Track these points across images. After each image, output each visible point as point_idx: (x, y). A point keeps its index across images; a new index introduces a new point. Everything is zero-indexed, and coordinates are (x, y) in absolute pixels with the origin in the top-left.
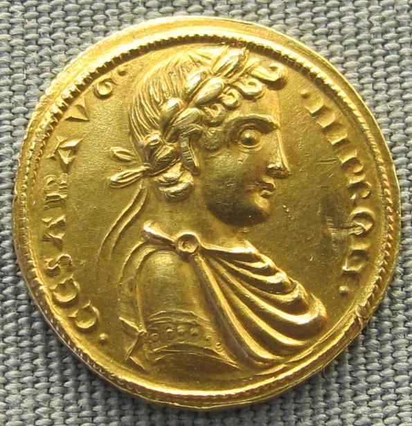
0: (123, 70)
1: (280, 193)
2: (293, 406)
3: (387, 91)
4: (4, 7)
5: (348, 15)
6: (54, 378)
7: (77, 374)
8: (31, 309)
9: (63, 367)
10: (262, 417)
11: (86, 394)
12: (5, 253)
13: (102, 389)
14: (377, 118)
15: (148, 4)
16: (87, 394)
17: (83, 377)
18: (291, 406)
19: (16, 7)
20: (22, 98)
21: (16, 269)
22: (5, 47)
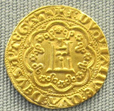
0: (26, 32)
1: (9, 69)
2: (82, 106)
3: (105, 24)
4: (1, 107)
5: (93, 8)
6: (12, 92)
7: (22, 100)
8: (7, 77)
9: (18, 97)
10: (74, 109)
11: (6, 78)
12: (1, 65)
13: (32, 106)
14: (103, 31)
15: (44, 1)
16: (20, 97)
17: (23, 101)
18: (81, 106)
19: (7, 5)
20: (8, 33)
21: (4, 67)
22: (2, 103)
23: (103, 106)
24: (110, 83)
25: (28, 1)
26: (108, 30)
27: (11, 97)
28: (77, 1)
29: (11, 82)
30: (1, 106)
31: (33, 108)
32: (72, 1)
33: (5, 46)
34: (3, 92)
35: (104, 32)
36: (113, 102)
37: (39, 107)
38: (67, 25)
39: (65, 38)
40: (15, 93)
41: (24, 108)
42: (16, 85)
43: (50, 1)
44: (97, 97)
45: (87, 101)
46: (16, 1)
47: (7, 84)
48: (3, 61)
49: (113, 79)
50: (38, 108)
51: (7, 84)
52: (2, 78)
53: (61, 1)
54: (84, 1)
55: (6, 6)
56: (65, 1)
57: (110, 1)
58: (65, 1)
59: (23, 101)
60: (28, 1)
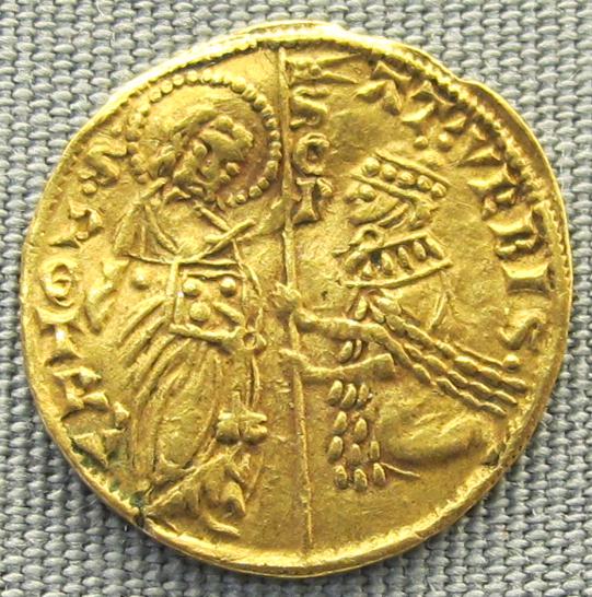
17: (152, 558)
22: (6, 83)
24: (553, 484)
26: (512, 27)
29: (30, 399)
30: (8, 69)
31: (203, 583)
32: (171, 5)
35: (530, 113)
38: (146, 353)
39: (172, 333)
40: (86, 509)
42: (51, 411)
44: (480, 526)
47: (28, 447)
49: (590, 466)
50: (227, 583)
51: (28, 447)
56: (561, 5)
58: (561, 5)
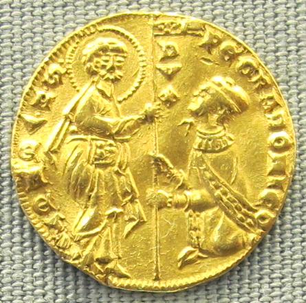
19: (293, 91)
23: (296, 248)
25: (181, 2)
27: (34, 262)
28: (88, 4)
33: (15, 109)
34: (12, 238)
36: (304, 227)
37: (135, 296)
41: (81, 295)
43: (140, 2)
45: (260, 244)
46: (233, 2)
48: (8, 179)
52: (6, 217)
53: (127, 2)
54: (130, 2)
55: (55, 30)
56: (255, 3)
57: (96, 2)
59: (80, 282)
60: (181, 2)
